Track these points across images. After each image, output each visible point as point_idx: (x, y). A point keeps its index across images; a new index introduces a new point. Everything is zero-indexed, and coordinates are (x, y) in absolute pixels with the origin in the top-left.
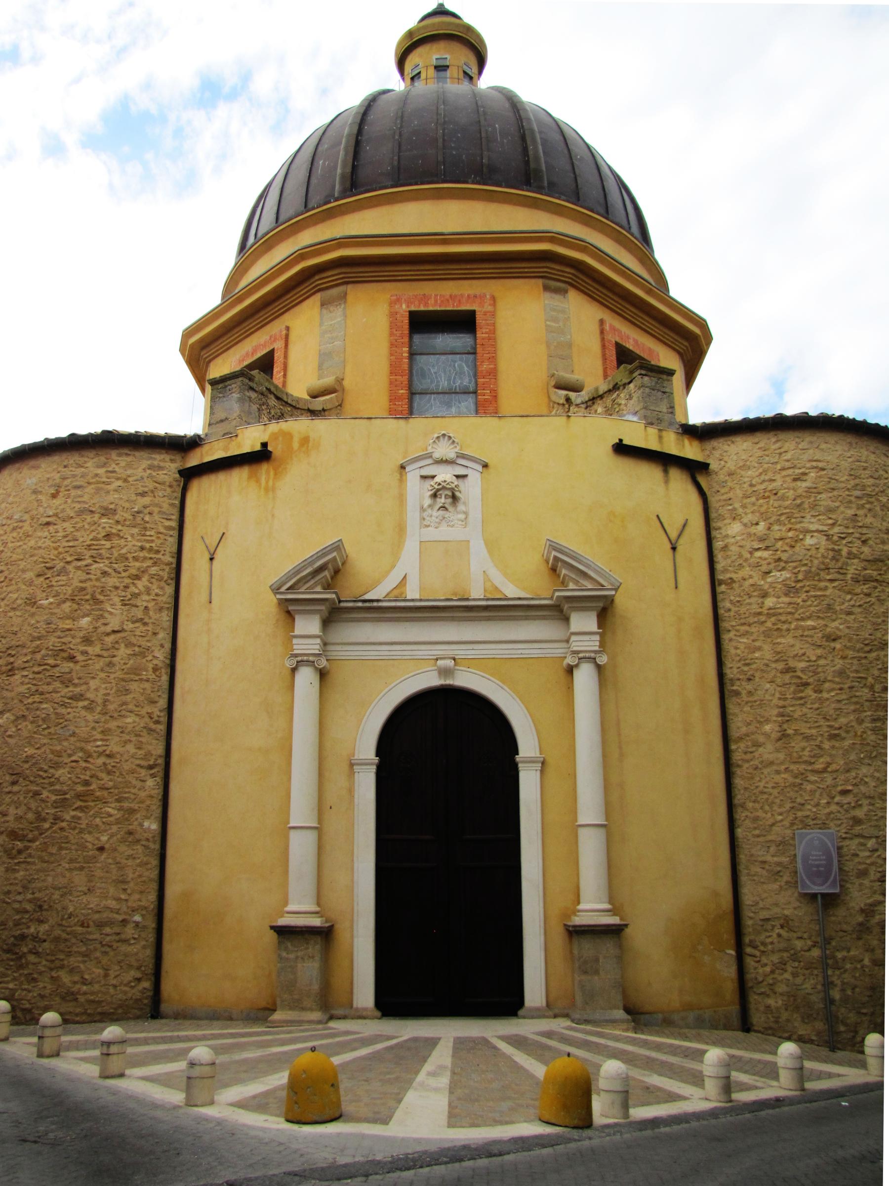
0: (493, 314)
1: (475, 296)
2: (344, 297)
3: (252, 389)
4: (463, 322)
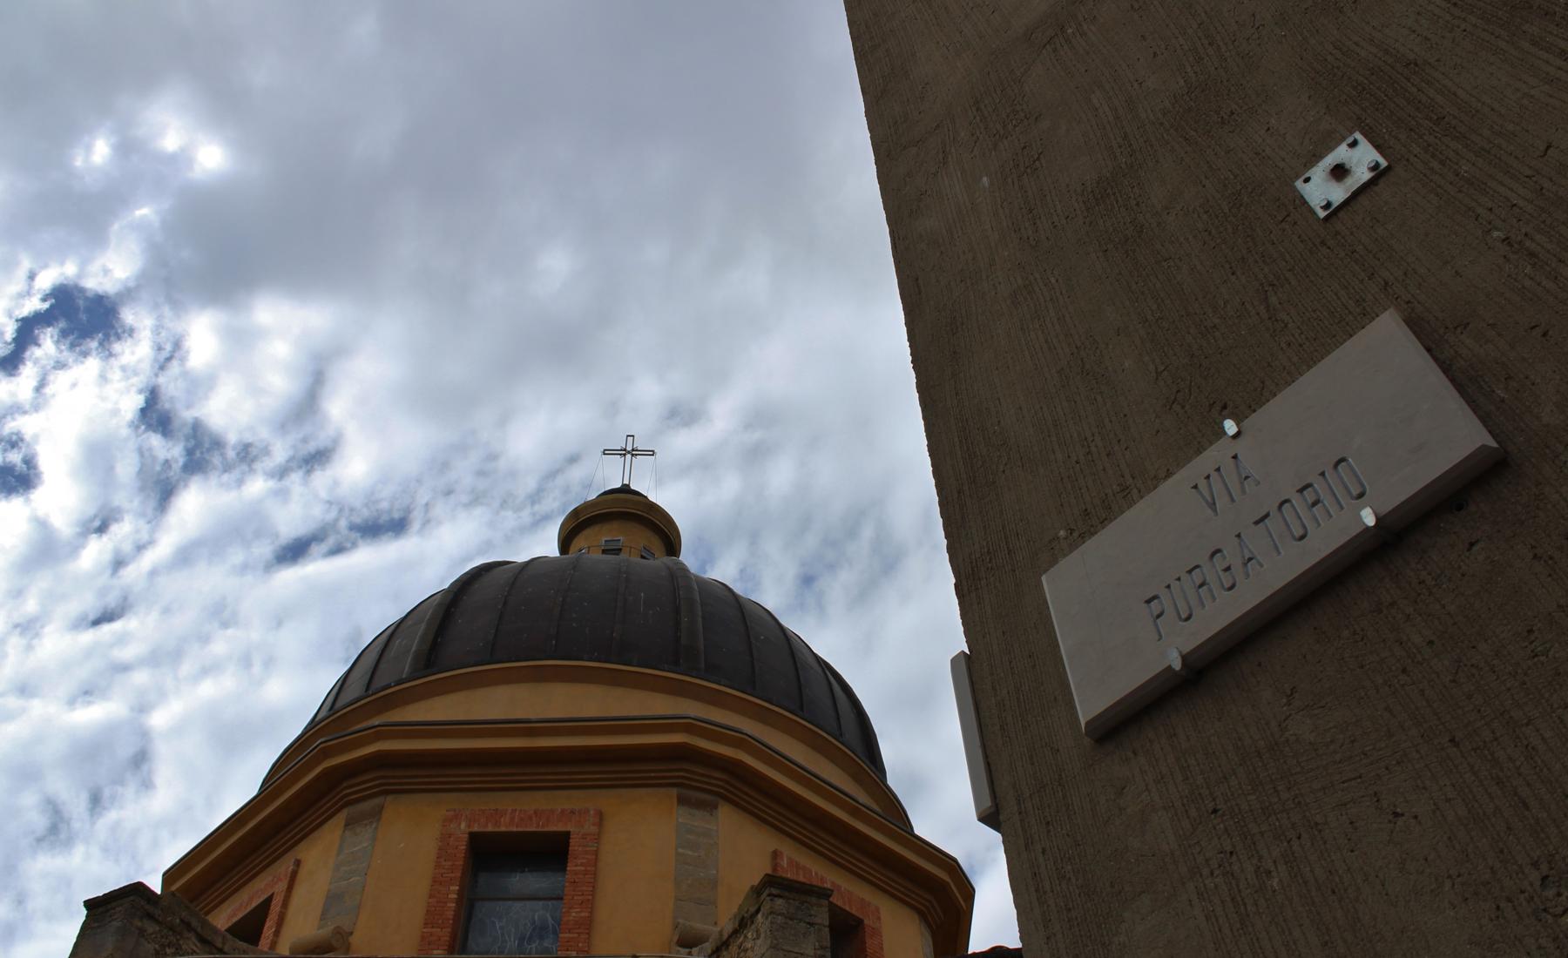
0: (598, 838)
1: (573, 812)
2: (377, 814)
3: (150, 917)
4: (549, 852)
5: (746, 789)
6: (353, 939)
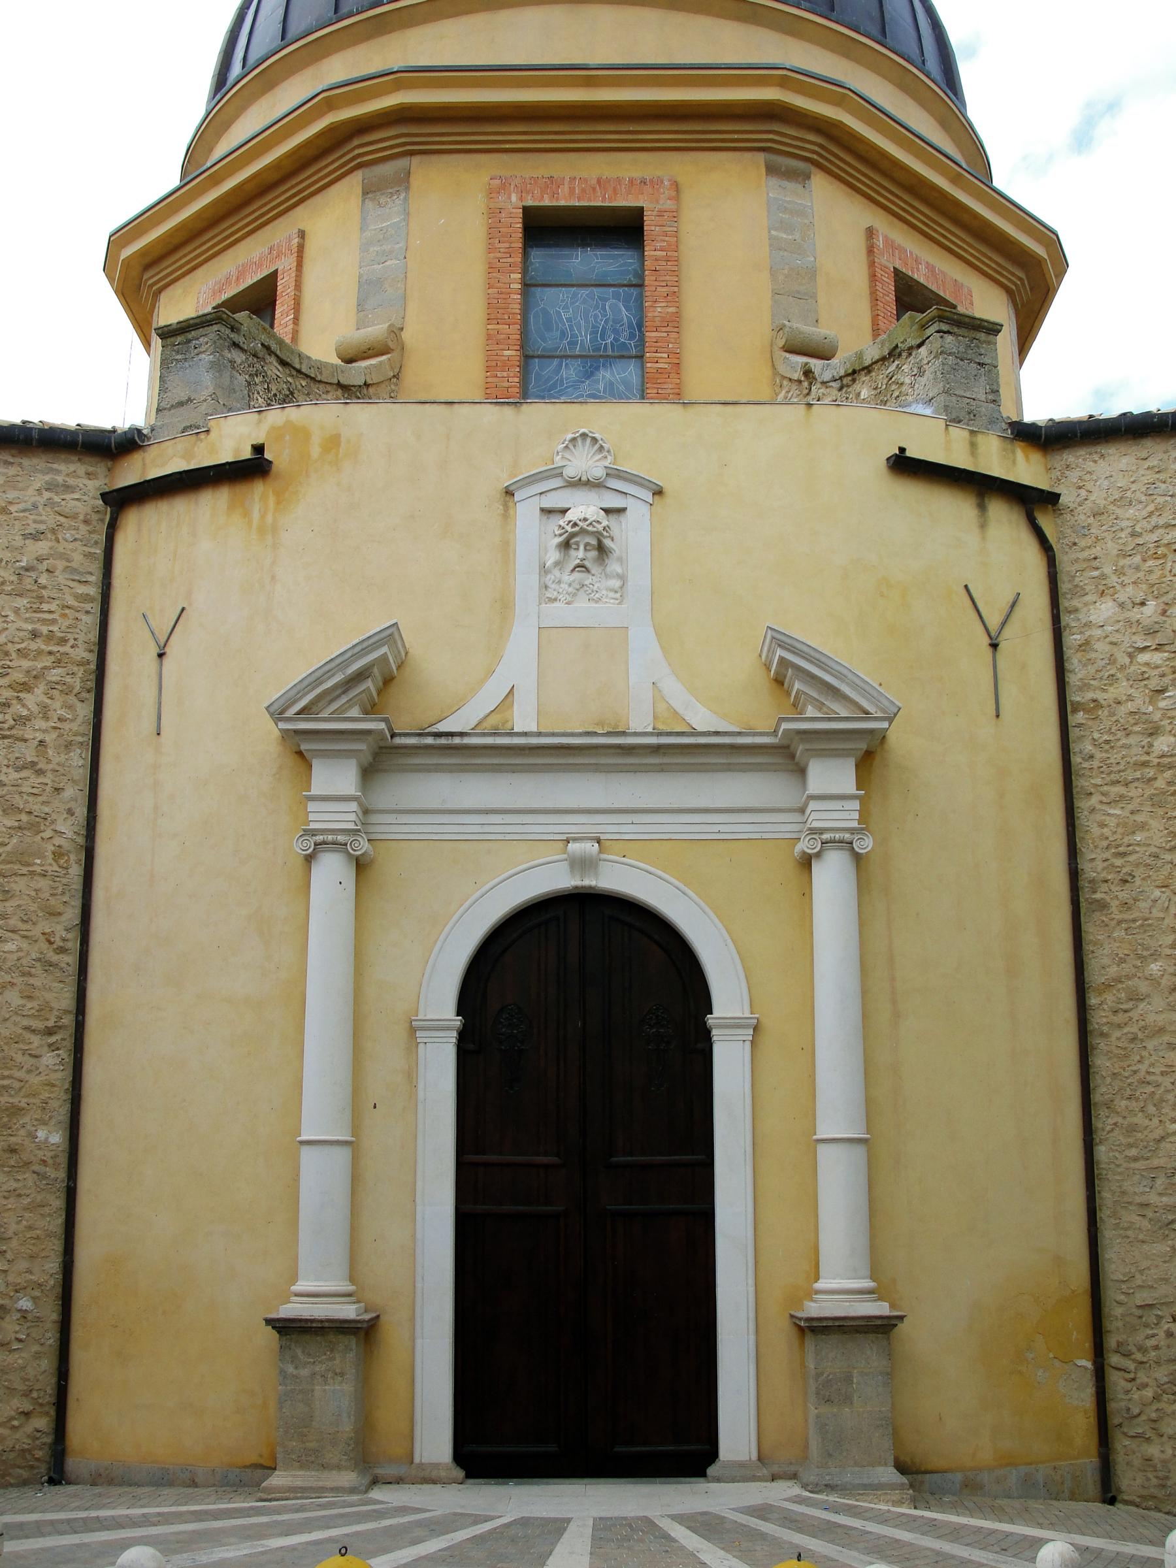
0: (675, 216)
1: (644, 182)
3: (236, 345)
4: (623, 229)
5: (916, 204)
6: (405, 335)
